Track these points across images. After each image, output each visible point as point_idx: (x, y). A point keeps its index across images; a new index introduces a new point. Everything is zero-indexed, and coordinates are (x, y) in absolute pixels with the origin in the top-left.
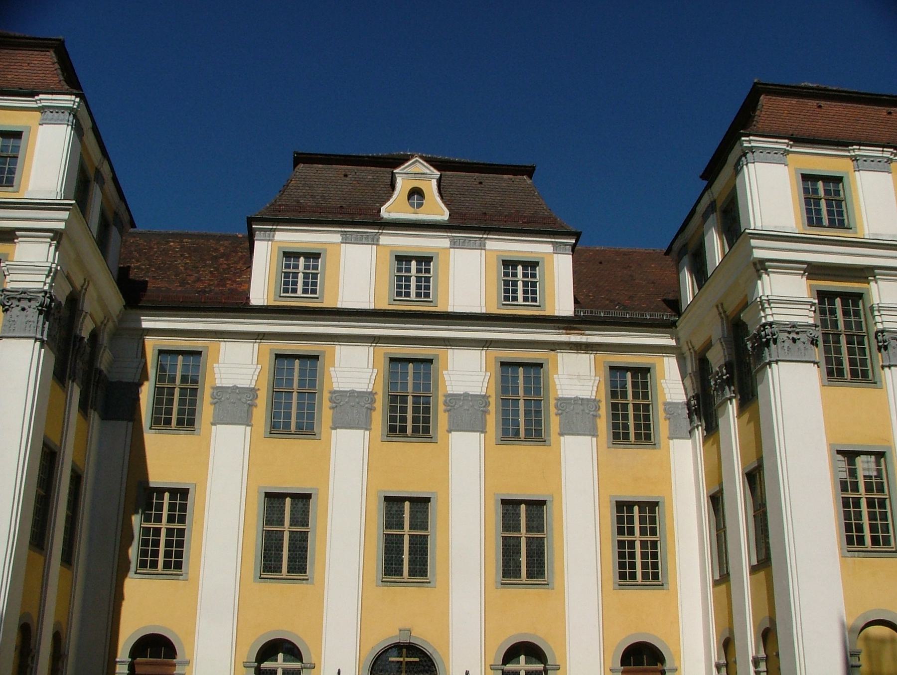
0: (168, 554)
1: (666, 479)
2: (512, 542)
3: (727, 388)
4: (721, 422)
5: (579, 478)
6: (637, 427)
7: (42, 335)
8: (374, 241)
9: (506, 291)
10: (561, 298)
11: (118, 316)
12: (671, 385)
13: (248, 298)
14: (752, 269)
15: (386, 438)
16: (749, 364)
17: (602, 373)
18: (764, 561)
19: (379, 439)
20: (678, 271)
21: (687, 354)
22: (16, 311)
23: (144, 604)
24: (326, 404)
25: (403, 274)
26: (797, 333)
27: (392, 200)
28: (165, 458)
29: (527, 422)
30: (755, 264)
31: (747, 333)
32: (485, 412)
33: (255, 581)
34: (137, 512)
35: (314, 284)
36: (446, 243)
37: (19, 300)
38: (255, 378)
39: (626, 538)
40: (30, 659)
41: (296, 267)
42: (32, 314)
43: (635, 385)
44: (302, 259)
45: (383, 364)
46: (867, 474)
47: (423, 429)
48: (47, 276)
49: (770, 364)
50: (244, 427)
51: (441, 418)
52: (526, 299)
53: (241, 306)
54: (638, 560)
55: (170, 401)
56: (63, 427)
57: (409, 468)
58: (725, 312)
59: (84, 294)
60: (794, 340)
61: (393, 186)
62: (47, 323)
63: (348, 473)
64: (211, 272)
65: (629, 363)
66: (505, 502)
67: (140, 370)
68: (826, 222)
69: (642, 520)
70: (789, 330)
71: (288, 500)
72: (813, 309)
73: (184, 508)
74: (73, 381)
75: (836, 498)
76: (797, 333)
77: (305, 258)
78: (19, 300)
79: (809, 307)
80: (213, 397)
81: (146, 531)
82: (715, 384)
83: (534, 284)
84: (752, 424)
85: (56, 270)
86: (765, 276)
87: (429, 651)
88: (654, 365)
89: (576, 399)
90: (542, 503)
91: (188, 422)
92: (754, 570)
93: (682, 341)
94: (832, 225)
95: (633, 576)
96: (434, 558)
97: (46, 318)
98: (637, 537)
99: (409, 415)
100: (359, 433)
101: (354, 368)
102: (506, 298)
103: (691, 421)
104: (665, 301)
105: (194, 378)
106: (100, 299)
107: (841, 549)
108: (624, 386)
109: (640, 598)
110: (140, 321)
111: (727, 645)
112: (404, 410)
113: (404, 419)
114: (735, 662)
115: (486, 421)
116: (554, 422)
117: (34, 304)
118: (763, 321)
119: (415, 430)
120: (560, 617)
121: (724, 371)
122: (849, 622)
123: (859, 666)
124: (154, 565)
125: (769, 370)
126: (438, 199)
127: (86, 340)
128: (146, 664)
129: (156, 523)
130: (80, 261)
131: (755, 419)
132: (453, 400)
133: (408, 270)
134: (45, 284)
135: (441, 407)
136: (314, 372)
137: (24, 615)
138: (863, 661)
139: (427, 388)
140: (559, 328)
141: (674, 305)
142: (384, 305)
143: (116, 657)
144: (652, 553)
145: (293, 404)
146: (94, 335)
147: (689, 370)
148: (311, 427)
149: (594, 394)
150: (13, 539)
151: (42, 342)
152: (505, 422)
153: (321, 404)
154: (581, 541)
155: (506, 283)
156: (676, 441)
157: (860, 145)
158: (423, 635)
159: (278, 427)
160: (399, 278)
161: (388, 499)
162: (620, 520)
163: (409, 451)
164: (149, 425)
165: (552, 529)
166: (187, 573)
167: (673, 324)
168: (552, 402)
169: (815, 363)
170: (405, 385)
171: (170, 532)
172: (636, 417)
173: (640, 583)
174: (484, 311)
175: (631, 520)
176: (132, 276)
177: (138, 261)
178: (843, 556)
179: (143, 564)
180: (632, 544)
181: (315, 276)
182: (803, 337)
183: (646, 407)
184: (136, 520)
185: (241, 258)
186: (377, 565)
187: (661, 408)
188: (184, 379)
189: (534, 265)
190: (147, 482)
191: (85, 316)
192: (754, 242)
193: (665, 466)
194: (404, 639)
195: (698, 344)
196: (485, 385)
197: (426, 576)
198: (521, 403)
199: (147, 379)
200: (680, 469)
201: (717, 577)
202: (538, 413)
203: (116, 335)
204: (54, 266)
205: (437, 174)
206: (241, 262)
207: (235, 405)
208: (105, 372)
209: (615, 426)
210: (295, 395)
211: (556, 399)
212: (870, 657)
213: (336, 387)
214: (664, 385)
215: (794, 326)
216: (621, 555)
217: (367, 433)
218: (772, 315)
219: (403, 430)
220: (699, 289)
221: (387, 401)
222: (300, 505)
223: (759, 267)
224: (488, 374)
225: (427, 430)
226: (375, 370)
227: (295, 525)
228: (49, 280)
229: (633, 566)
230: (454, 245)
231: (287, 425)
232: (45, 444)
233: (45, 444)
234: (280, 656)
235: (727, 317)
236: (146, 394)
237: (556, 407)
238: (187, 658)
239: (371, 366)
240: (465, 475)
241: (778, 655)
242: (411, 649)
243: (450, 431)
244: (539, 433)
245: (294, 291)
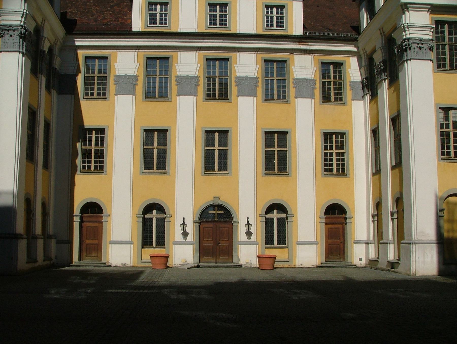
0: (96, 162)
1: (349, 121)
2: (270, 153)
3: (383, 73)
4: (379, 91)
5: (305, 119)
6: (335, 94)
7: (23, 50)
9: (267, 22)
10: (296, 26)
11: (62, 39)
12: (354, 72)
13: (131, 28)
14: (400, 9)
16: (395, 61)
17: (318, 66)
18: (398, 164)
20: (359, 11)
21: (363, 56)
22: (7, 37)
23: (86, 188)
24: (174, 83)
25: (213, 13)
26: (422, 44)
28: (92, 113)
29: (278, 91)
30: (402, 6)
31: (395, 44)
32: (256, 86)
33: (140, 174)
34: (79, 141)
35: (166, 19)
37: (8, 31)
38: (137, 70)
39: (329, 151)
40: (32, 215)
41: (156, 10)
42: (16, 38)
43: (334, 72)
44: (158, 6)
45: (203, 61)
46: (454, 120)
47: (224, 95)
48: (22, 17)
49: (406, 61)
50: (131, 96)
51: (234, 89)
52: (278, 26)
53: (127, 32)
54: (334, 162)
55: (93, 84)
56: (38, 103)
57: (217, 115)
58: (384, 33)
59: (43, 27)
60: (420, 48)
62: (25, 43)
63: (186, 118)
64: (110, 14)
65: (332, 60)
66: (266, 133)
67: (76, 68)
69: (337, 142)
70: (418, 42)
71: (156, 133)
72: (432, 30)
73: (103, 138)
74: (41, 74)
75: (437, 131)
76: (422, 44)
77: (160, 5)
78: (8, 31)
79: (430, 29)
80: (115, 81)
81: (84, 151)
82: (377, 72)
83: (282, 18)
84: (395, 93)
85: (27, 13)
86: (406, 13)
87: (229, 208)
88: (345, 61)
89: (304, 79)
90: (286, 133)
91: (102, 94)
92: (393, 168)
93: (360, 48)
95: (332, 170)
96: (230, 165)
97: (24, 41)
98: (334, 151)
99: (217, 88)
100: (192, 97)
101: (188, 64)
102: (267, 26)
103: (364, 91)
104: (351, 27)
105: (105, 71)
106: (52, 30)
107: (438, 158)
108: (329, 72)
109: (335, 181)
110: (74, 41)
111: (378, 205)
112: (214, 85)
113: (214, 90)
114: (382, 214)
115: (257, 90)
116: (292, 91)
117: (17, 33)
118: (404, 37)
119: (220, 95)
120: (295, 191)
121: (382, 64)
122: (440, 194)
123: (443, 216)
124: (89, 168)
125: (406, 64)
127: (46, 52)
128: (88, 217)
129: (89, 148)
130: (39, 9)
131: (397, 91)
132: (240, 80)
134: (21, 22)
135: (234, 84)
136: (167, 66)
137: (26, 194)
138: (445, 214)
139: (226, 74)
140: (295, 42)
141: (357, 29)
143: (73, 214)
144: (342, 159)
145: (157, 83)
146: (50, 49)
147: (363, 64)
148: (166, 95)
149: (313, 76)
150: (18, 157)
151: (24, 55)
152: (267, 91)
153: (171, 86)
154: (305, 152)
155: (267, 17)
156: (355, 102)
158: (226, 200)
159: (149, 95)
160: (211, 15)
161: (207, 132)
162: (325, 142)
163: (217, 106)
164: (82, 96)
165: (291, 147)
166: (106, 171)
167: (356, 40)
168: (291, 81)
169: (431, 60)
170: (214, 72)
171: (96, 151)
172: (335, 89)
173: (335, 174)
174: (256, 33)
175: (331, 142)
176: (68, 17)
177: (70, 9)
178: (439, 162)
179: (84, 168)
180: (331, 154)
181: (166, 15)
182: (425, 46)
183: (340, 84)
184: (79, 145)
185: (126, 6)
187: (348, 84)
188: (100, 72)
190: (84, 126)
191: (45, 39)
192: (408, 5)
193: (350, 114)
194: (216, 202)
195: (369, 49)
196: (256, 72)
197: (227, 170)
198: (275, 81)
199: (80, 72)
200: (357, 116)
201: (374, 171)
202: (284, 86)
203: (62, 49)
204: (25, 11)
206: (127, 8)
207: (127, 85)
208: (58, 69)
209: (324, 93)
210: (157, 79)
212: (449, 212)
213: (178, 74)
214: (350, 72)
215: (421, 40)
216: (326, 160)
217: (195, 97)
218: (409, 34)
219: (214, 96)
220: (371, 20)
222: (162, 135)
223: (404, 7)
224: (258, 66)
225: (226, 96)
226: (199, 65)
227: (160, 146)
228: (23, 19)
229: (332, 165)
231: (154, 95)
232: (29, 108)
233: (30, 108)
234: (154, 211)
235: (385, 35)
236: (80, 80)
237: (293, 83)
238: (108, 213)
239: (197, 62)
240: (246, 119)
241: (403, 210)
242: (220, 207)
243: (238, 96)
244: (284, 97)
245: (155, 23)
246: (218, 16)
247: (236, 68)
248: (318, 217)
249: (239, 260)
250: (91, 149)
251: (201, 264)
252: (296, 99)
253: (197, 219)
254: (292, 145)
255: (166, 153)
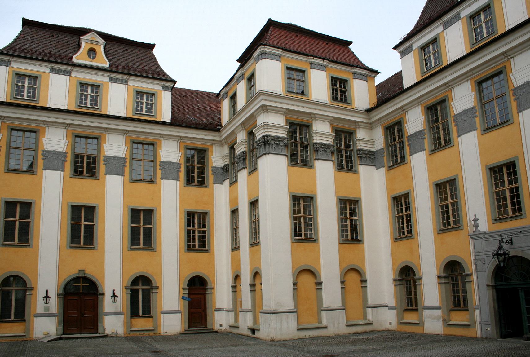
1: (211, 202)
8: (68, 73)
15: (72, 176)
19: (69, 176)
24: (210, 172)
27: (78, 53)
32: (124, 166)
36: (107, 79)
50: (60, 172)
57: (84, 191)
60: (278, 144)
61: (79, 46)
68: (339, 99)
69: (199, 221)
90: (152, 211)
94: (342, 100)
100: (58, 172)
101: (55, 140)
107: (292, 239)
111: (237, 277)
113: (82, 167)
119: (88, 172)
120: (159, 265)
126: (104, 56)
133: (142, 99)
142: (131, 115)
156: (47, 171)
157: (314, 57)
158: (91, 272)
160: (81, 95)
161: (73, 207)
162: (188, 220)
169: (286, 155)
178: (292, 242)
186: (67, 239)
189: (152, 95)
194: (82, 275)
196: (125, 152)
205: (104, 42)
211: (42, 151)
213: (46, 148)
217: (62, 173)
219: (82, 172)
221: (73, 157)
225: (94, 173)
226: (67, 141)
230: (112, 80)
240: (113, 197)
242: (86, 279)
243: (106, 174)
246: (89, 97)
247: (105, 147)
248: (124, 288)
249: (105, 330)
250: (15, 221)
251: (64, 336)
252: (44, 171)
253: (61, 291)
254: (158, 222)
255: (151, 231)
